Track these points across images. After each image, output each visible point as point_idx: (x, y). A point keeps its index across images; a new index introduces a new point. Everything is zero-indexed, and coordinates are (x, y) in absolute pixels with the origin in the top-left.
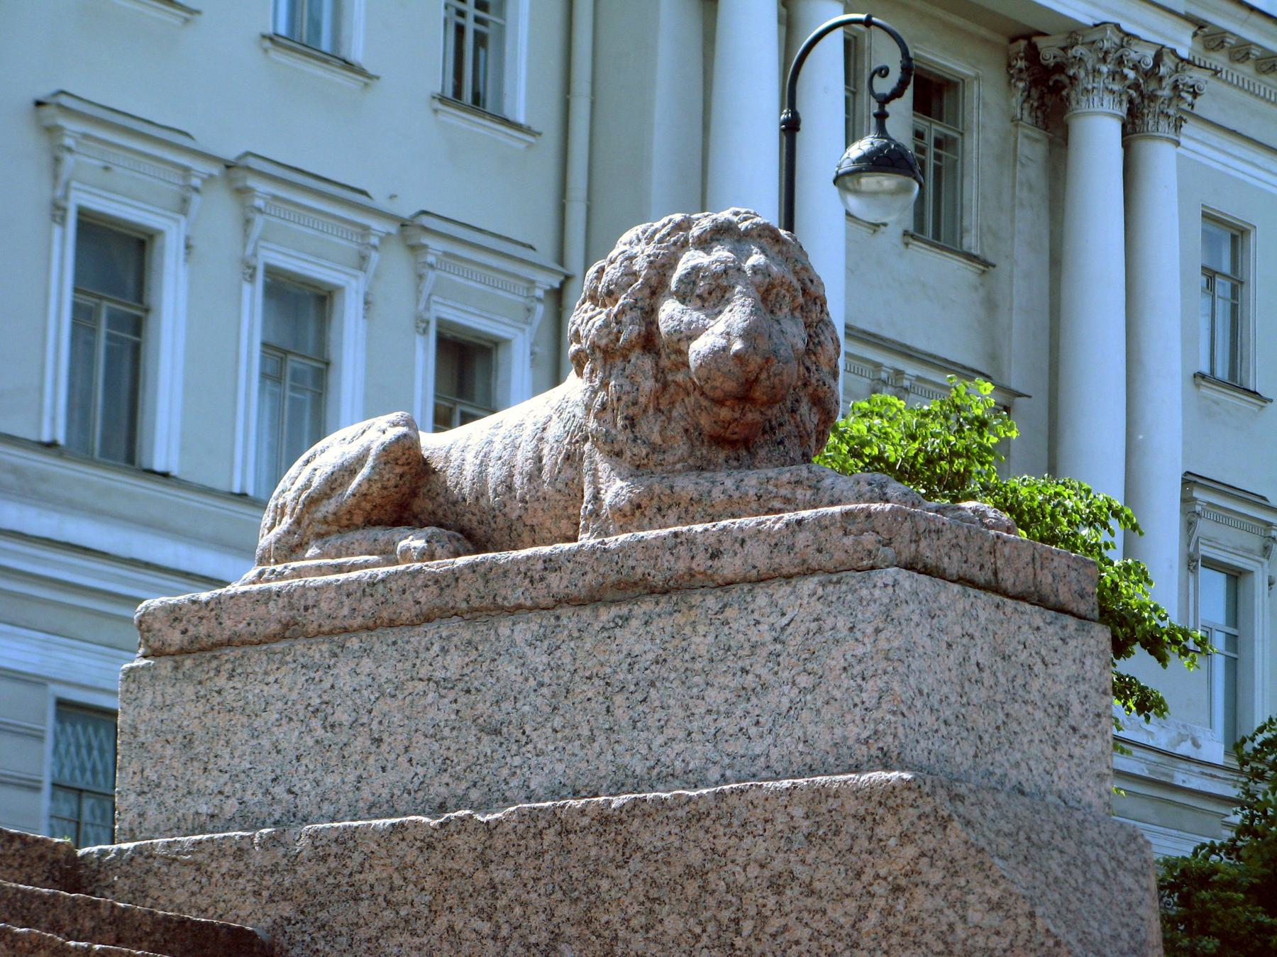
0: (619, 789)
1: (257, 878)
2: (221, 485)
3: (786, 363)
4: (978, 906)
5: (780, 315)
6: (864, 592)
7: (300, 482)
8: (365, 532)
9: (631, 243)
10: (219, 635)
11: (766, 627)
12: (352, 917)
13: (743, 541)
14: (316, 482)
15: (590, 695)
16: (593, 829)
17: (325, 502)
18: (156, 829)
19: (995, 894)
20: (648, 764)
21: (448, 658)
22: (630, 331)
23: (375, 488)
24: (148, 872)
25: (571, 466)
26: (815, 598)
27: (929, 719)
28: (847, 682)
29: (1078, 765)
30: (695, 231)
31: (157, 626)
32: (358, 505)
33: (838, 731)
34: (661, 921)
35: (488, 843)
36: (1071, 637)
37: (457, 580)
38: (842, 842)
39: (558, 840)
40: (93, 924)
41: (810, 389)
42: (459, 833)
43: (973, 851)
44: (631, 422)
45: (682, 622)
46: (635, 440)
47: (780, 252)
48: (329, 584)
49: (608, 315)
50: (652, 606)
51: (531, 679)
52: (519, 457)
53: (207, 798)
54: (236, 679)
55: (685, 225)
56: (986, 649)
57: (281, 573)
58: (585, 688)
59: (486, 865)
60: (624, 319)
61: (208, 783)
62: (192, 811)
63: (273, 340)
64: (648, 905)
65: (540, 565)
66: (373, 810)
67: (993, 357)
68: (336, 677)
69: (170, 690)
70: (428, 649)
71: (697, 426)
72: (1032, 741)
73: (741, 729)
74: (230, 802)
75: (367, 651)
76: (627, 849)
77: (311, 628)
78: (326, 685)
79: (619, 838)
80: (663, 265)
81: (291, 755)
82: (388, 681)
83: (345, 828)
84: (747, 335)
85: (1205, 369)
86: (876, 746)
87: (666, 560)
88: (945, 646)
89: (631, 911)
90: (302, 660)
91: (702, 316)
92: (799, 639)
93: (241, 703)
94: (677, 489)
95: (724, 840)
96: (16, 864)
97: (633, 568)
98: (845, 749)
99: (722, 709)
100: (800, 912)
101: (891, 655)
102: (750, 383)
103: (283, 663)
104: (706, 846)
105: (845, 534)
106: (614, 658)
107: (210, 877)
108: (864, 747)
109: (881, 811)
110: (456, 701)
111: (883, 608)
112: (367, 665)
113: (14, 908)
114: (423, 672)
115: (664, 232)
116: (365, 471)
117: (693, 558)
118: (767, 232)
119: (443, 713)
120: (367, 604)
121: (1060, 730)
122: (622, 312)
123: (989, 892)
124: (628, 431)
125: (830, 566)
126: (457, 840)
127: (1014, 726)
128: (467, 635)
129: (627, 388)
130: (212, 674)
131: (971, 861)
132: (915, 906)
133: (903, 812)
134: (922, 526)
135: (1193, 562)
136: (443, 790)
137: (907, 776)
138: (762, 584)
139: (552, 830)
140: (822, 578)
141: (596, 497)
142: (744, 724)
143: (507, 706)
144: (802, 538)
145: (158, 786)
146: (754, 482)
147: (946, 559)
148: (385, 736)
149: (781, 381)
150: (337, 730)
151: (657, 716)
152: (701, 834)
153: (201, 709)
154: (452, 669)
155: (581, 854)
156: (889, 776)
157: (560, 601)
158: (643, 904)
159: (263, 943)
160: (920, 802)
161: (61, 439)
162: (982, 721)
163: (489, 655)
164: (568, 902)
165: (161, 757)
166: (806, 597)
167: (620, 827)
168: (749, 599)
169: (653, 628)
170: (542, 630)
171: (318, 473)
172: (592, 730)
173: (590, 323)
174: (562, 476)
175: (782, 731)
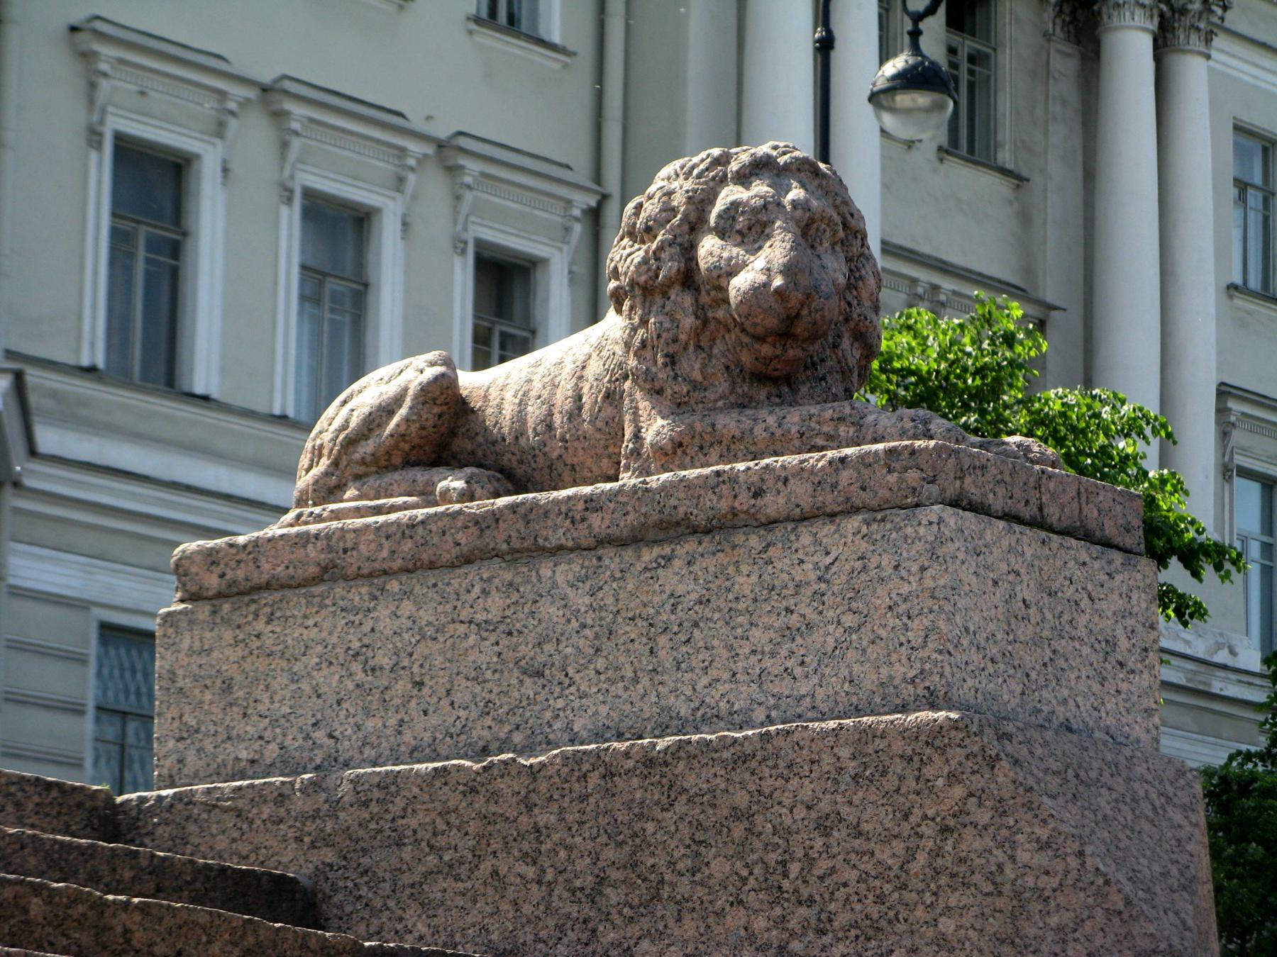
0: (663, 731)
1: (298, 824)
2: (261, 408)
4: (1027, 846)
5: (821, 249)
6: (909, 530)
7: (337, 424)
8: (404, 473)
9: (669, 178)
10: (258, 578)
11: (811, 566)
12: (394, 862)
13: (786, 480)
14: (353, 424)
15: (633, 636)
16: (638, 772)
17: (363, 443)
18: (196, 774)
19: (1043, 833)
20: (692, 705)
21: (490, 600)
22: (669, 268)
23: (414, 428)
24: (188, 819)
25: (611, 404)
26: (859, 536)
27: (975, 657)
28: (892, 622)
29: (1126, 701)
31: (194, 570)
32: (396, 446)
33: (884, 671)
34: (707, 864)
35: (531, 787)
36: (1117, 571)
37: (497, 521)
38: (890, 783)
39: (603, 783)
40: (132, 874)
41: (852, 325)
42: (502, 777)
43: (1021, 791)
44: (672, 360)
46: (675, 378)
48: (367, 526)
49: (647, 252)
51: (574, 621)
52: (558, 396)
53: (247, 743)
54: (275, 623)
55: (724, 160)
56: (1032, 585)
57: (319, 516)
58: (628, 629)
59: (530, 808)
61: (248, 728)
62: (232, 756)
63: (309, 263)
64: (694, 847)
65: (581, 506)
66: (415, 754)
67: (1028, 270)
68: (377, 619)
69: (208, 635)
70: (469, 591)
71: (738, 363)
73: (786, 670)
74: (270, 747)
75: (407, 594)
76: (673, 791)
77: (351, 571)
78: (366, 628)
79: (664, 781)
81: (332, 699)
82: (429, 624)
83: (387, 773)
85: (1238, 279)
86: (922, 685)
87: (709, 500)
90: (341, 603)
91: (742, 252)
92: (844, 579)
93: (281, 647)
94: (719, 427)
95: (770, 781)
96: (54, 813)
97: (675, 507)
98: (891, 689)
99: (767, 649)
100: (848, 853)
101: (936, 594)
102: (792, 319)
103: (322, 606)
105: (889, 472)
106: (657, 599)
107: (251, 822)
108: (910, 687)
109: (928, 751)
110: (497, 643)
112: (407, 607)
114: (465, 615)
115: (702, 167)
116: (403, 411)
117: (735, 497)
118: (806, 167)
119: (485, 656)
120: (407, 546)
122: (661, 248)
124: (669, 368)
125: (875, 503)
126: (501, 784)
128: (508, 576)
129: (667, 325)
130: (250, 618)
131: (1019, 799)
132: (964, 847)
134: (967, 462)
135: (1227, 472)
136: (485, 733)
139: (596, 773)
141: (637, 436)
142: (789, 664)
143: (549, 648)
144: (846, 476)
145: (197, 731)
146: (796, 419)
147: (991, 496)
148: (426, 680)
149: (823, 316)
150: (378, 673)
151: (701, 657)
152: (747, 776)
153: (240, 654)
154: (494, 610)
155: (627, 797)
157: (603, 541)
158: (689, 846)
160: (967, 741)
162: (1029, 659)
163: (531, 597)
164: (613, 845)
167: (665, 769)
168: (793, 538)
169: (695, 568)
171: (355, 414)
172: (635, 672)
173: (629, 260)
174: (603, 414)
175: (827, 671)
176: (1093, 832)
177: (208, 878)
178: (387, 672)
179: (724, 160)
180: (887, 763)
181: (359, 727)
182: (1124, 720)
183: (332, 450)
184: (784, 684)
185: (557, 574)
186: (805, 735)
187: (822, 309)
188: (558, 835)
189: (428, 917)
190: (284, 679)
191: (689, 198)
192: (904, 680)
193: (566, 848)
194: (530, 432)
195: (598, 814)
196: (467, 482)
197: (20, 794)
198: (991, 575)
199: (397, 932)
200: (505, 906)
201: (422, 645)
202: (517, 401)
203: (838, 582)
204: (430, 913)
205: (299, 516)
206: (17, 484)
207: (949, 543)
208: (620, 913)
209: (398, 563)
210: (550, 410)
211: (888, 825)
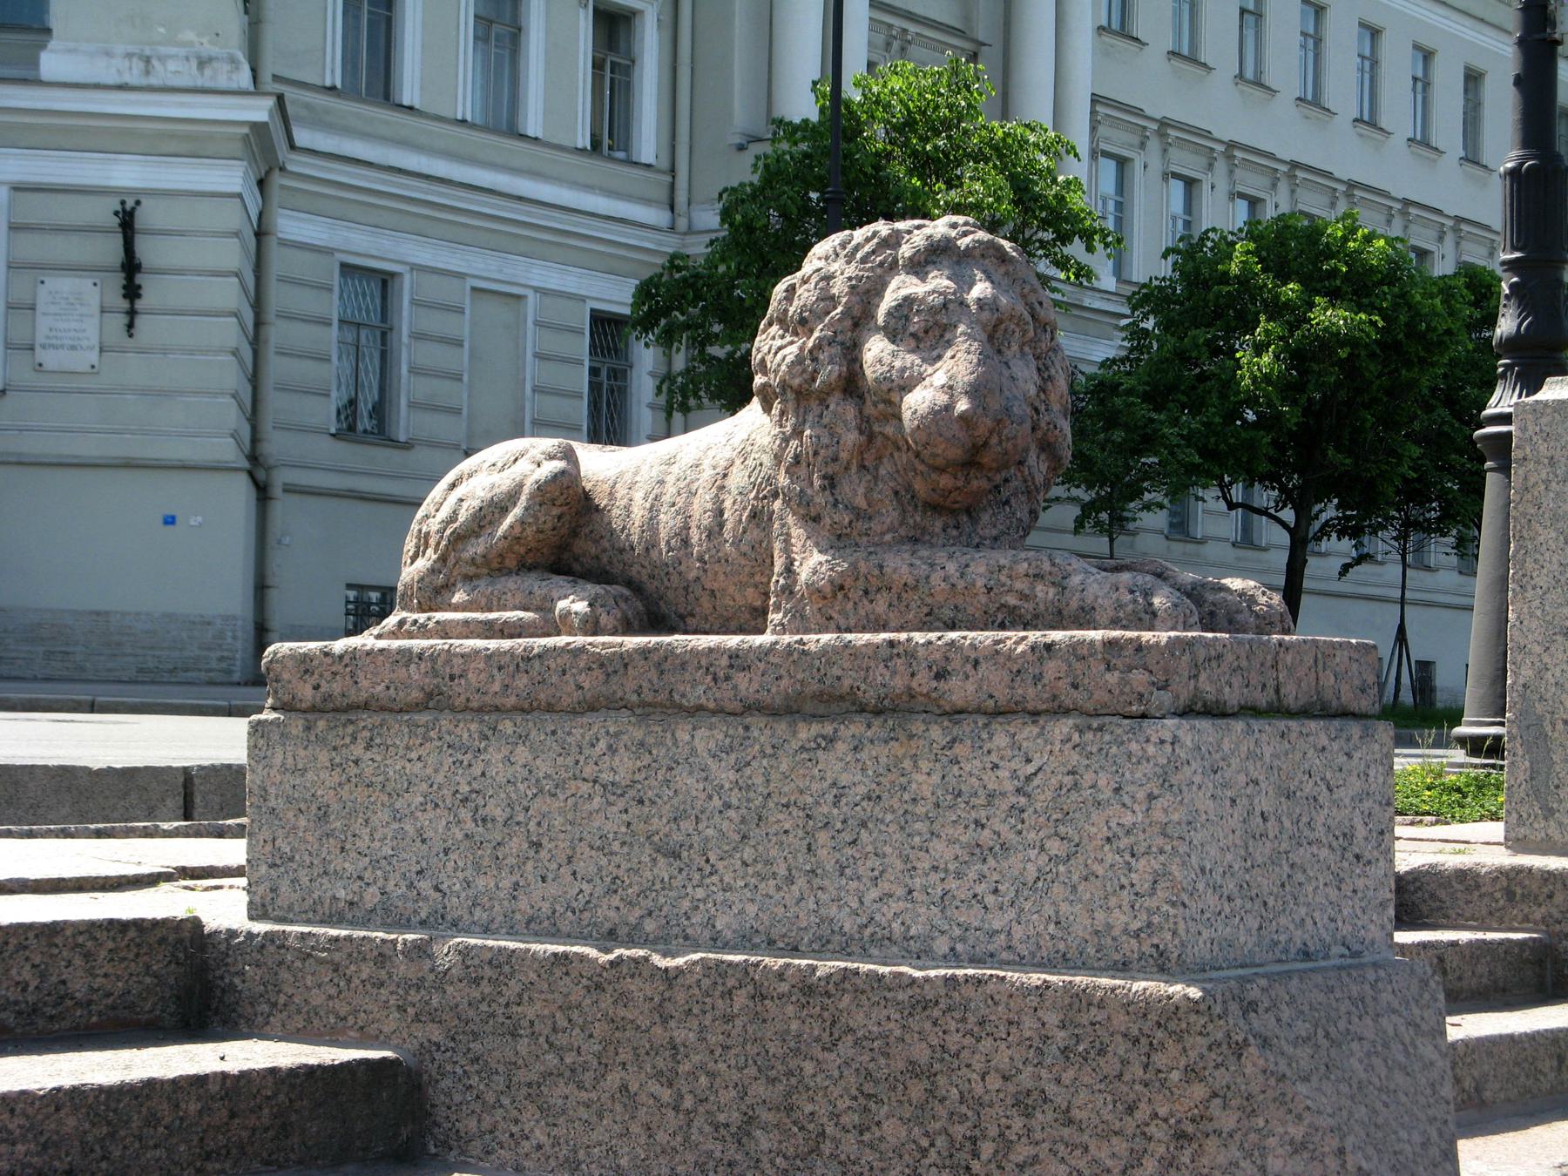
0: (822, 948)
1: (401, 992)
2: (449, 114)
3: (1020, 424)
4: (1280, 1151)
5: (1009, 354)
6: (1134, 746)
7: (444, 513)
8: (519, 579)
9: (827, 258)
10: (355, 696)
11: (1007, 774)
12: (510, 1055)
13: (976, 663)
14: (461, 518)
15: (787, 826)
16: (794, 999)
17: (473, 540)
18: (290, 908)
19: (1297, 1132)
20: (859, 921)
21: (617, 759)
22: (828, 372)
23: (529, 531)
24: (281, 963)
25: (758, 526)
26: (1069, 745)
27: (1212, 900)
28: (1110, 857)
29: (1361, 900)
30: (906, 251)
31: (286, 676)
32: (510, 549)
33: (1100, 916)
34: (878, 1124)
35: (667, 995)
36: (1356, 748)
37: (626, 666)
38: (1110, 1065)
39: (751, 1005)
40: (199, 1105)
41: (1039, 434)
42: (632, 976)
43: (1272, 1082)
44: (831, 482)
45: (900, 754)
46: (835, 505)
47: (1007, 273)
48: (477, 652)
49: (801, 349)
50: (863, 729)
51: (716, 798)
52: (695, 506)
53: (345, 882)
54: (375, 750)
55: (893, 240)
56: (1271, 793)
57: (424, 626)
58: (781, 817)
59: (665, 1019)
60: (821, 357)
61: (347, 865)
62: (329, 894)
63: (483, 13)
64: (861, 1100)
65: (724, 661)
66: (535, 927)
67: (967, 18)
68: (488, 763)
69: (302, 753)
70: (593, 745)
71: (909, 487)
72: (1317, 888)
73: (975, 896)
74: (371, 890)
75: (523, 738)
76: (836, 1032)
77: (459, 702)
78: (477, 771)
79: (826, 1014)
80: (868, 291)
81: (439, 846)
82: (547, 776)
83: (500, 949)
84: (976, 391)
85: (1104, 23)
86: (1149, 942)
87: (880, 674)
88: (1228, 803)
89: (842, 1104)
90: (447, 738)
91: (918, 361)
92: (1049, 795)
93: (381, 778)
94: (887, 570)
95: (957, 1037)
96: (131, 956)
97: (839, 678)
98: (1109, 941)
99: (951, 867)
100: (1055, 1143)
101: (1169, 831)
102: (978, 448)
103: (427, 738)
104: (935, 1042)
105: (1108, 669)
106: (815, 786)
107: (349, 981)
108: (1133, 941)
109: (1160, 1034)
110: (626, 811)
111: (1159, 770)
112: (522, 754)
113: (97, 1114)
114: (589, 771)
115: (867, 248)
116: (516, 512)
117: (913, 675)
118: (992, 252)
119: (612, 823)
120: (522, 682)
121: (1345, 864)
122: (818, 346)
123: (1292, 1130)
124: (827, 492)
125: (1090, 706)
126: (632, 985)
127: (1300, 877)
128: (638, 734)
129: (825, 440)
130: (347, 740)
131: (1270, 1094)
132: (1205, 1161)
133: (1189, 1041)
134: (1202, 654)
135: (1095, 154)
136: (612, 914)
137: (1194, 993)
138: (1000, 719)
139: (743, 992)
140: (1078, 721)
141: (789, 570)
142: (979, 889)
143: (687, 825)
144: (1052, 668)
145: (292, 859)
146: (982, 569)
147: (1227, 689)
148: (544, 841)
149: (1015, 446)
150: (489, 825)
151: (869, 864)
152: (928, 1025)
153: (337, 779)
154: (622, 771)
155: (780, 1026)
156: (1171, 990)
157: (751, 708)
158: (855, 1098)
159: (409, 1069)
160: (1210, 1027)
161: (339, 85)
162: (1265, 882)
163: (666, 762)
164: (763, 1080)
165: (294, 828)
166: (1057, 743)
167: (826, 1001)
168: (985, 736)
169: (863, 755)
170: (728, 740)
171: (465, 505)
172: (790, 870)
173: (779, 356)
174: (748, 537)
175: (1027, 905)
176: (1351, 1114)
177: (293, 1086)
178: (499, 825)
179: (893, 240)
180: (1107, 1040)
181: (468, 884)
182: (1360, 923)
183: (438, 543)
184: (972, 912)
185: (697, 740)
186: (1001, 988)
187: (1015, 437)
188: (698, 1057)
189: (547, 1125)
190: (385, 815)
191: (853, 287)
192: (1125, 931)
193: (707, 1074)
194: (663, 544)
195: (745, 1042)
196: (590, 605)
197: (89, 944)
198: (1229, 794)
199: (512, 1135)
200: (635, 1129)
201: (538, 800)
202: (648, 505)
203: (1043, 798)
204: (550, 1120)
205: (402, 623)
206: (282, 169)
207: (1186, 767)
208: (772, 1163)
209: (511, 701)
210: (686, 522)
211: (1109, 1117)
